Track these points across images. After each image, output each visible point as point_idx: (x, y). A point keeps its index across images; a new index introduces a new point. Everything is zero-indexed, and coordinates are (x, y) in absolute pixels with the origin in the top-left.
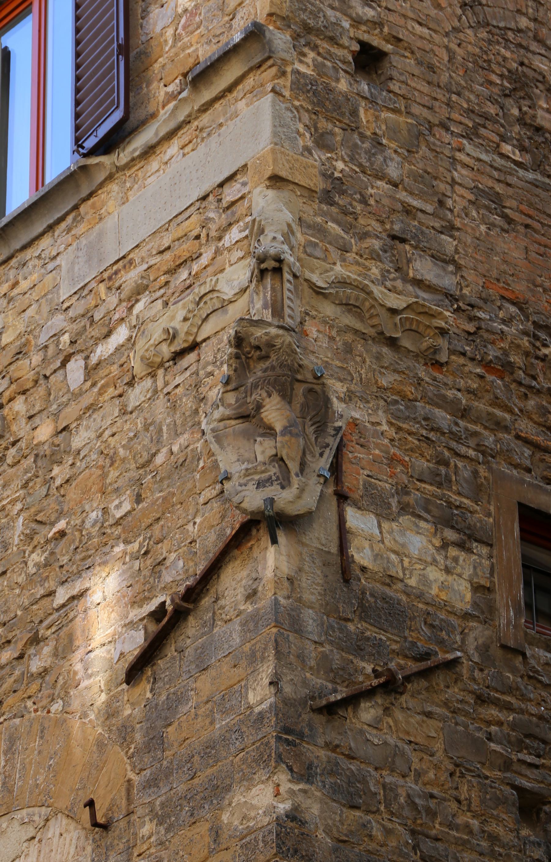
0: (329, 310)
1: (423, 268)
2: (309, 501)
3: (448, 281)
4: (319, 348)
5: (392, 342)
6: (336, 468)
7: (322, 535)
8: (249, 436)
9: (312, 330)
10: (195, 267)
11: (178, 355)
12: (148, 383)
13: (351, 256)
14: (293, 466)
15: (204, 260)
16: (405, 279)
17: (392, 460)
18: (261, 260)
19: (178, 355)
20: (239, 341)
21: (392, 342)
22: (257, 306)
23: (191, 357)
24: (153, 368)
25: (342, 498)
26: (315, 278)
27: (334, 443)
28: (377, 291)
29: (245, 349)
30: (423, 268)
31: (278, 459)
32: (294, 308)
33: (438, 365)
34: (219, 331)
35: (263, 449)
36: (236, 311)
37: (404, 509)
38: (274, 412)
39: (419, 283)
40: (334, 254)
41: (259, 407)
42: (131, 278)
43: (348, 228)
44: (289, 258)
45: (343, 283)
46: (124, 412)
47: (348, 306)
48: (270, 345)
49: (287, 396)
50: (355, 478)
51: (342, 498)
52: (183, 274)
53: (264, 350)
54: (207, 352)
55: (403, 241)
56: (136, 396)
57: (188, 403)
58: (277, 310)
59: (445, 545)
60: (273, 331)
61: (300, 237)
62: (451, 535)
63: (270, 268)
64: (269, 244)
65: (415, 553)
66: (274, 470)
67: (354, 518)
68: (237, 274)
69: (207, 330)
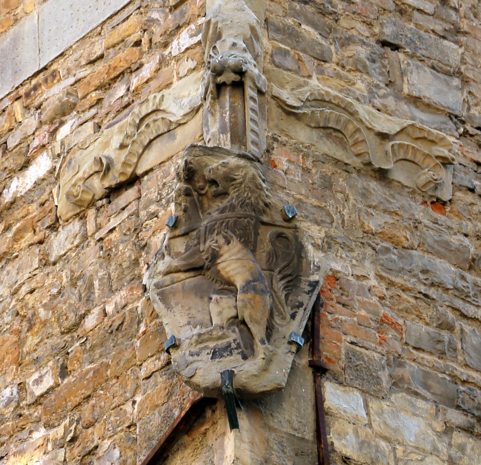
0: (302, 134)
1: (421, 81)
2: (278, 375)
3: (453, 98)
4: (290, 185)
5: (382, 175)
6: (312, 333)
7: (293, 416)
8: (202, 293)
9: (282, 160)
10: (135, 81)
11: (113, 192)
12: (75, 226)
13: (330, 67)
14: (258, 331)
15: (146, 72)
16: (399, 96)
17: (383, 322)
18: (217, 72)
19: (113, 192)
20: (189, 174)
21: (382, 175)
22: (212, 129)
23: (130, 194)
24: (82, 208)
25: (319, 370)
26: (286, 95)
27: (309, 302)
28: (363, 111)
29: (197, 184)
30: (421, 81)
31: (237, 321)
32: (258, 132)
33: (439, 204)
34: (164, 161)
35: (220, 309)
36: (185, 136)
37: (397, 383)
38: (234, 263)
39: (415, 100)
40: (310, 64)
41: (215, 256)
42: (53, 94)
43: (327, 32)
44: (253, 70)
45: (321, 101)
46: (45, 263)
47: (328, 130)
48: (229, 179)
49: (250, 243)
50: (336, 346)
51: (319, 370)
52: (120, 90)
53: (221, 185)
54: (149, 188)
55: (396, 48)
56: (60, 243)
57: (126, 252)
58: (238, 135)
59: (448, 430)
60: (233, 161)
61: (266, 43)
62: (457, 418)
63: (228, 82)
64: (228, 52)
65: (411, 439)
66: (233, 336)
67: (334, 396)
68: (187, 90)
69: (150, 159)
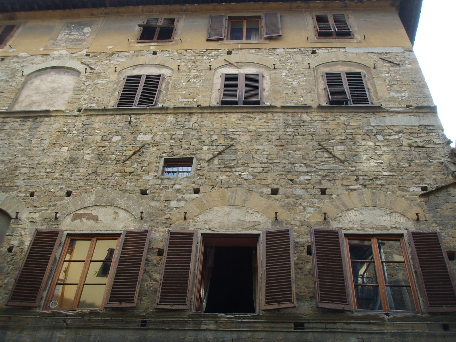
42: (397, 129)
